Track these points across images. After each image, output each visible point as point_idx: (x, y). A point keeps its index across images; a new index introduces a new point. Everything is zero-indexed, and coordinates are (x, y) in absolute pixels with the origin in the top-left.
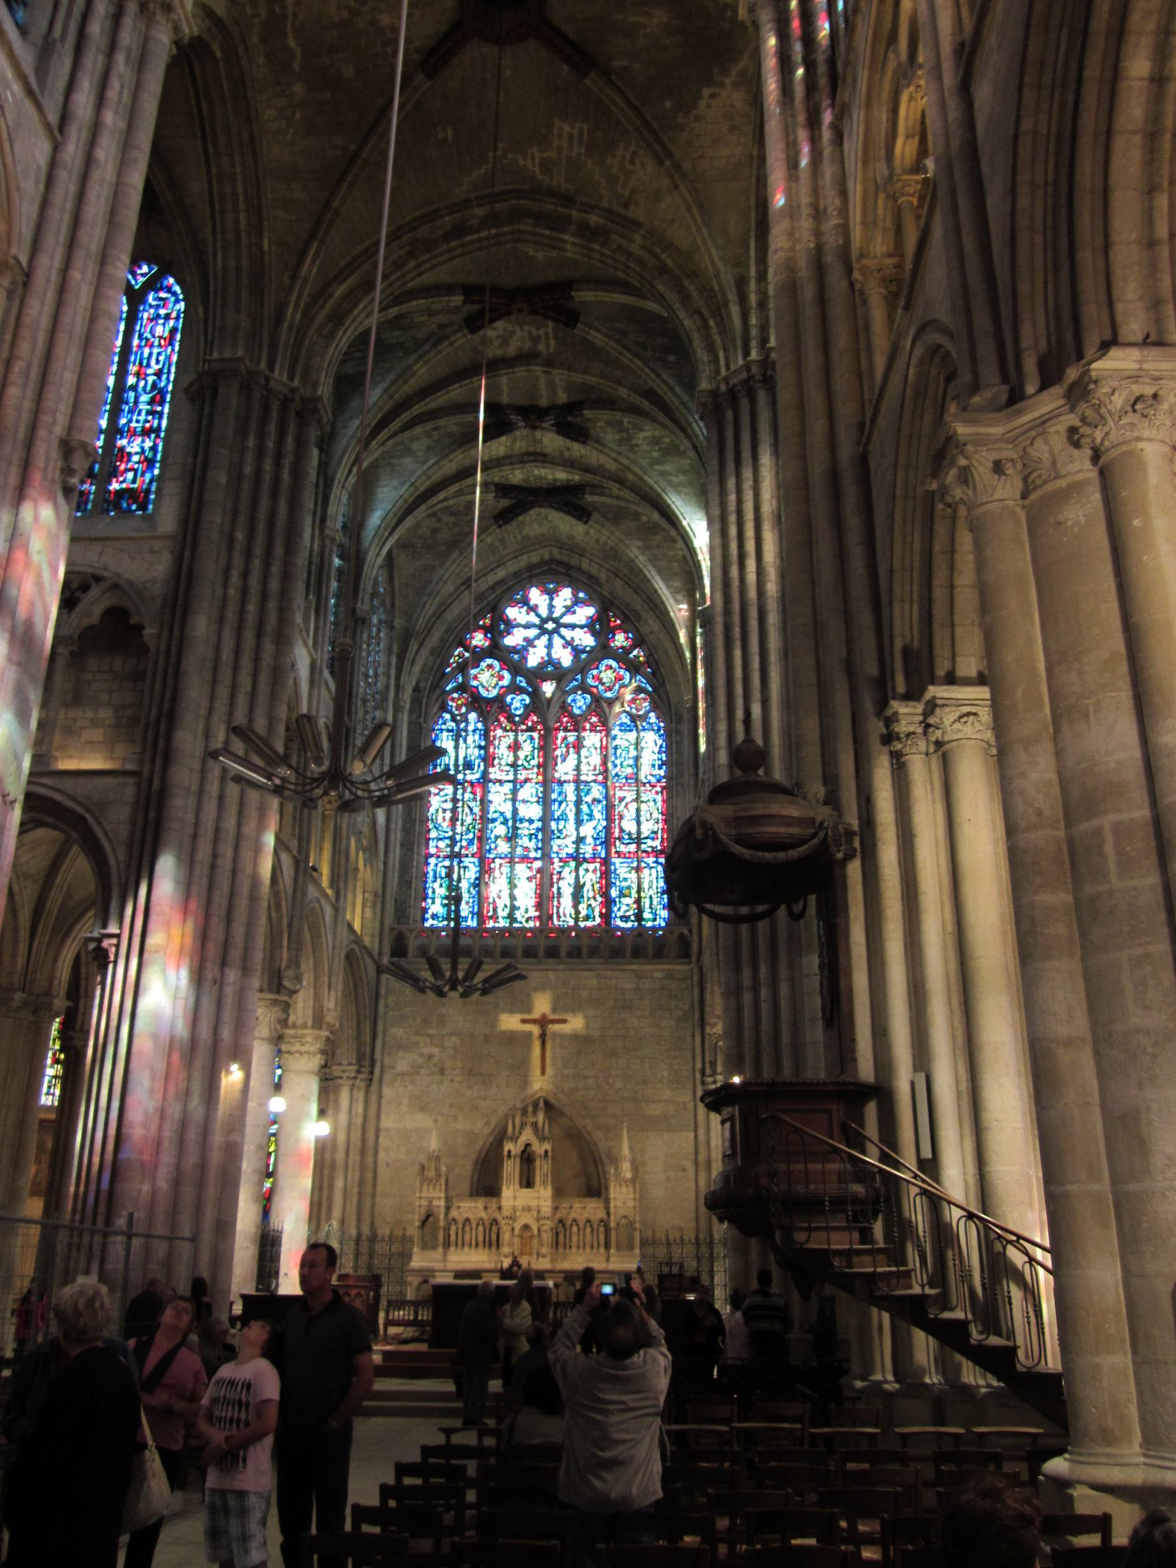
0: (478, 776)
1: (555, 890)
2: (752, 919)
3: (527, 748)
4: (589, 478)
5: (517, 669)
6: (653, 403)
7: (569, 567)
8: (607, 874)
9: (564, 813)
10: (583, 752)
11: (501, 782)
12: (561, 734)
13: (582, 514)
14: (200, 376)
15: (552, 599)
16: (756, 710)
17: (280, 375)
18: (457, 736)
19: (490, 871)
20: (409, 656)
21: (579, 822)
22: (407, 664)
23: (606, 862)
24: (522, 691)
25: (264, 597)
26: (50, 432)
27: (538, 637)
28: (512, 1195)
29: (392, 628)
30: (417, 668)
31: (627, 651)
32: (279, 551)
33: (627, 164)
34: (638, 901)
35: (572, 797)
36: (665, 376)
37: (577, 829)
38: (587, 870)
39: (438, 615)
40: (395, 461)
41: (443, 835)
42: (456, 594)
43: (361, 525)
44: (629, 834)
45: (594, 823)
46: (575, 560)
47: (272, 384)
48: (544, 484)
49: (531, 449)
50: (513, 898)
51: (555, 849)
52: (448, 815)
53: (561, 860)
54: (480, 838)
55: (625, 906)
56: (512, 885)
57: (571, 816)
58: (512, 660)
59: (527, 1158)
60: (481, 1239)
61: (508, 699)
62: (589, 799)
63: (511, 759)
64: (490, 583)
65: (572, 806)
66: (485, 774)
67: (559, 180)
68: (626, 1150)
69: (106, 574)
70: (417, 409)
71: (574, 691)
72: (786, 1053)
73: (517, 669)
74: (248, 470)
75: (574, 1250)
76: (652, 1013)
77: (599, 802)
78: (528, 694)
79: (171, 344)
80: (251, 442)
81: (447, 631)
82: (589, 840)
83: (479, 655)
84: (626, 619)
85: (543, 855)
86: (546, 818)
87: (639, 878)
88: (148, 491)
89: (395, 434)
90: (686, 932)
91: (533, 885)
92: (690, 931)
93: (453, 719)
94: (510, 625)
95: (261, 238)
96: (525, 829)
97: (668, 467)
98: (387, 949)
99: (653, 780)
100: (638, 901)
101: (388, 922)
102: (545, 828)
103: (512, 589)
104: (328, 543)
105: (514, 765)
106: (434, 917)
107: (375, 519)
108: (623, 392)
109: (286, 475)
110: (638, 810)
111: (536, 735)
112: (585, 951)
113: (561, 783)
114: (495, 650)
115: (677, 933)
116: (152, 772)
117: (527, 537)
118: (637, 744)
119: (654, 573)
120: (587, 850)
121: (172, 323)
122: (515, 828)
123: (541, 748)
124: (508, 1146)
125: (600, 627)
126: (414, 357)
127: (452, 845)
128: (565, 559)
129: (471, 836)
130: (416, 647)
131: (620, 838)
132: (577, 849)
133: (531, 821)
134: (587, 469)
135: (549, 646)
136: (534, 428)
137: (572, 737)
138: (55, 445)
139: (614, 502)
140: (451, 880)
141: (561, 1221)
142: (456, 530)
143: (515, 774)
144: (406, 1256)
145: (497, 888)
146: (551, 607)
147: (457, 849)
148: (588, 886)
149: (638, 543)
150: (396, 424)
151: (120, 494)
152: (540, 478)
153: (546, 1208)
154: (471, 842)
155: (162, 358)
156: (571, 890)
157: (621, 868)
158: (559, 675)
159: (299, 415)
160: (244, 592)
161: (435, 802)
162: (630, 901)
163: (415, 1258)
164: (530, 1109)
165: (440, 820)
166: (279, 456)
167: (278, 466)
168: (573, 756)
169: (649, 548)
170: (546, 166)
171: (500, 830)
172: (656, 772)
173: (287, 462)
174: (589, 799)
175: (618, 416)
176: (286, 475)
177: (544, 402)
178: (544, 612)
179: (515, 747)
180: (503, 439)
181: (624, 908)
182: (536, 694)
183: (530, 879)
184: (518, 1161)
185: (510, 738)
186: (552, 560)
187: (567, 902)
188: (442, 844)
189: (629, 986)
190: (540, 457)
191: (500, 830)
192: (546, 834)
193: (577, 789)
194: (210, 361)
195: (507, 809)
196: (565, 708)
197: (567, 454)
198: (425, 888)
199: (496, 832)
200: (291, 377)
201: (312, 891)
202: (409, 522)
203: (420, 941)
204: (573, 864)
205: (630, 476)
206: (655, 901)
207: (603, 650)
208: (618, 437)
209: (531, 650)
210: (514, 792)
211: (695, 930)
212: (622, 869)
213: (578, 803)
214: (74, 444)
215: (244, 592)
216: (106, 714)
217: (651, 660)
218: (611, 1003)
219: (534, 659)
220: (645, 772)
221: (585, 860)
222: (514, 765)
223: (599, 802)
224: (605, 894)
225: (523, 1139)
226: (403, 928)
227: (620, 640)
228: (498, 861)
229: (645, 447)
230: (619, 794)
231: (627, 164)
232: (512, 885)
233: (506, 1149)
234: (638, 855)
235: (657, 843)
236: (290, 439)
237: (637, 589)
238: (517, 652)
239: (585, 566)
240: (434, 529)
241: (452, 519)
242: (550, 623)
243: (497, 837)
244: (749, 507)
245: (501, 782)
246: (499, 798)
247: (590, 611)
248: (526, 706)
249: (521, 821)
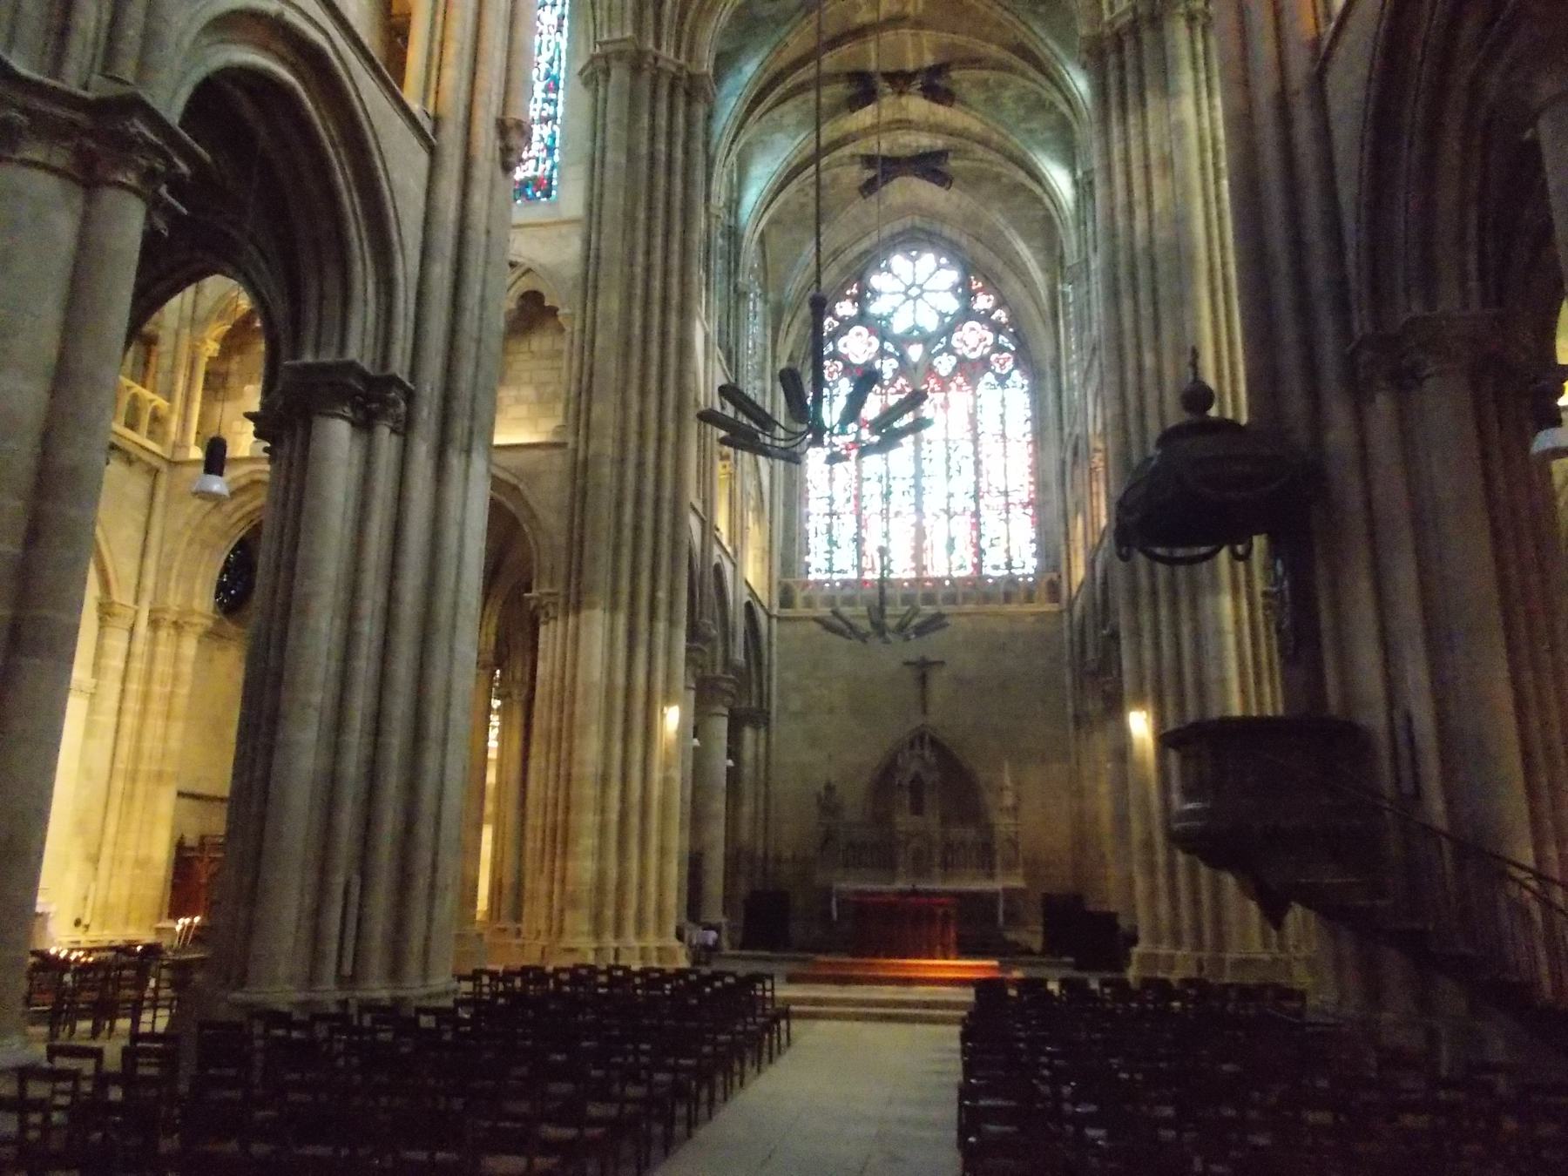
2: (1192, 561)
4: (954, 141)
5: (883, 336)
6: (1023, 58)
7: (930, 234)
13: (942, 179)
14: (593, 59)
16: (1149, 360)
17: (667, 52)
20: (784, 326)
22: (782, 334)
24: (891, 355)
25: (666, 274)
26: (488, 112)
29: (766, 302)
30: (791, 338)
31: (989, 313)
32: (677, 229)
36: (1036, 29)
40: (766, 138)
43: (738, 202)
46: (937, 227)
47: (661, 63)
48: (907, 152)
49: (898, 116)
58: (880, 329)
68: (1007, 781)
69: (519, 260)
70: (790, 83)
71: (939, 353)
72: (1190, 691)
74: (644, 149)
79: (559, 31)
80: (645, 121)
83: (846, 325)
84: (986, 279)
88: (550, 179)
89: (770, 109)
94: (876, 294)
96: (897, 487)
97: (1034, 125)
98: (776, 601)
101: (776, 574)
103: (871, 259)
104: (713, 220)
106: (818, 570)
108: (993, 50)
109: (679, 154)
112: (960, 599)
114: (862, 318)
116: (577, 442)
120: (956, 505)
121: (558, 10)
122: (889, 487)
125: (966, 294)
126: (787, 27)
128: (927, 227)
134: (951, 133)
136: (901, 93)
138: (492, 122)
139: (977, 164)
150: (770, 99)
151: (524, 184)
152: (905, 146)
155: (552, 45)
158: (927, 340)
159: (688, 94)
160: (648, 269)
164: (917, 743)
166: (670, 135)
167: (670, 144)
173: (679, 141)
175: (985, 74)
176: (679, 154)
177: (910, 67)
180: (870, 108)
182: (902, 359)
186: (913, 228)
190: (905, 124)
194: (601, 44)
196: (931, 370)
197: (932, 119)
200: (677, 55)
201: (716, 551)
202: (782, 197)
203: (805, 593)
205: (995, 137)
207: (967, 314)
208: (983, 97)
211: (1064, 577)
212: (992, 525)
214: (509, 123)
215: (648, 269)
216: (528, 392)
217: (1014, 318)
226: (790, 581)
227: (983, 302)
229: (1011, 105)
236: (680, 119)
237: (998, 253)
240: (810, 197)
242: (914, 288)
244: (1135, 153)
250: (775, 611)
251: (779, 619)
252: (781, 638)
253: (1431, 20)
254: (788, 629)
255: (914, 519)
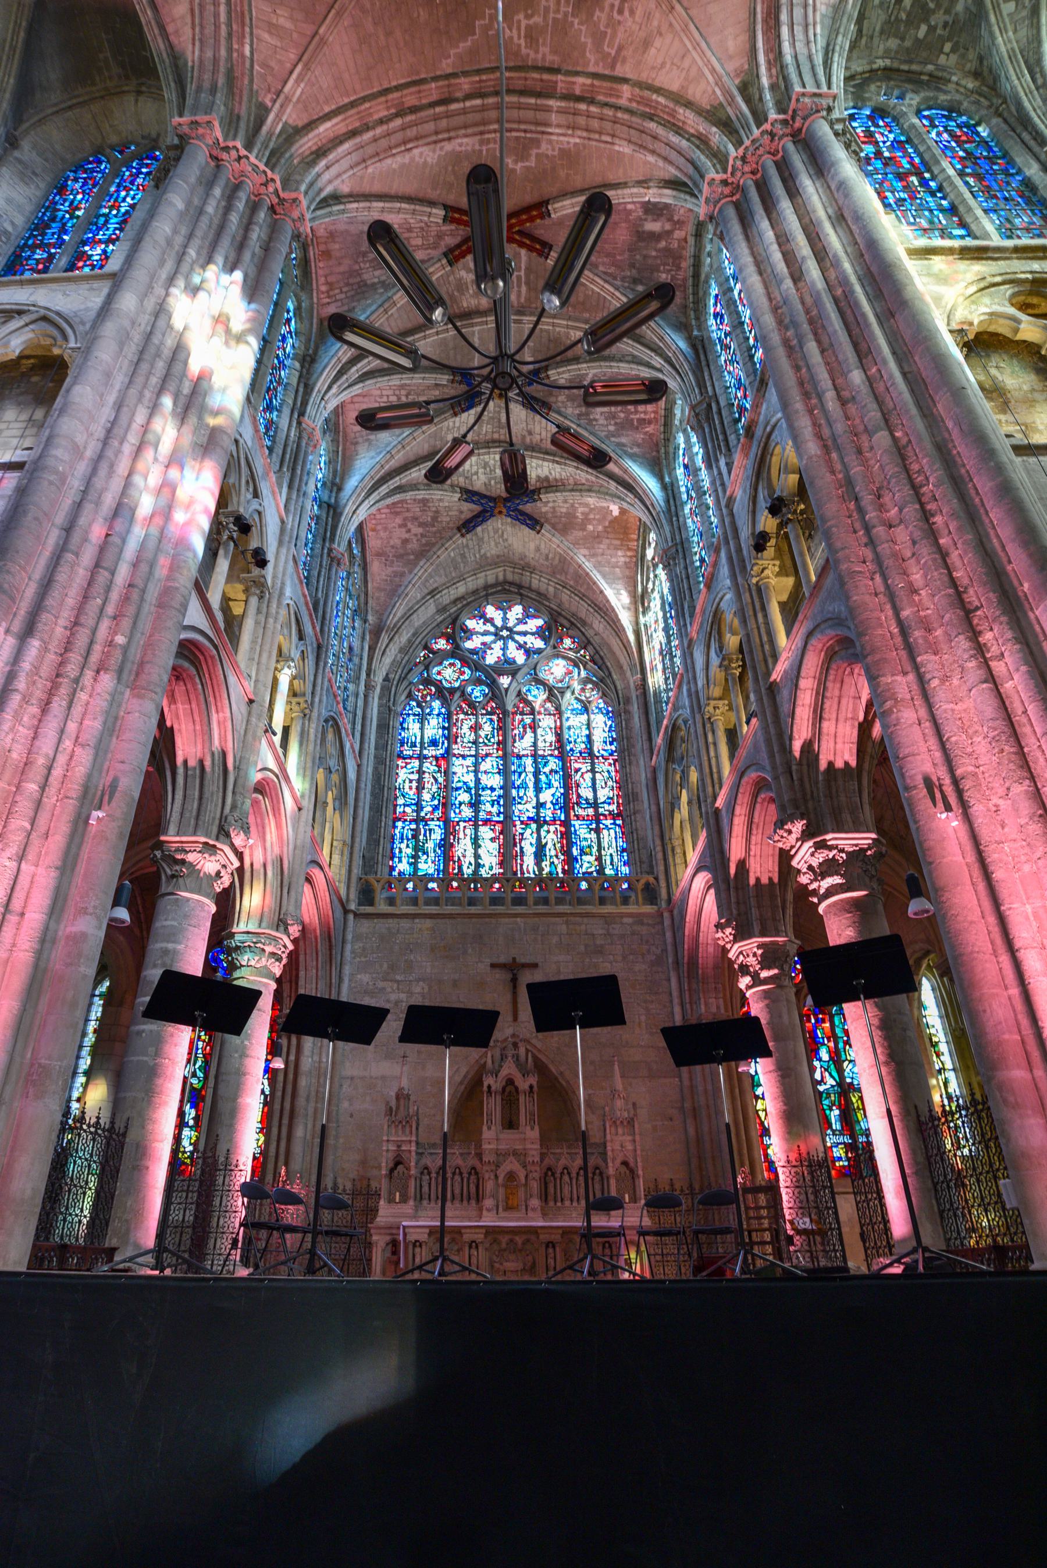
0: (442, 751)
1: (518, 849)
3: (487, 728)
5: (477, 667)
8: (567, 836)
9: (524, 782)
10: (539, 731)
11: (464, 757)
12: (518, 717)
15: (505, 614)
18: (422, 719)
19: (455, 833)
21: (538, 790)
23: (566, 824)
27: (494, 642)
28: (492, 1137)
33: (615, 14)
34: (599, 859)
35: (530, 769)
37: (537, 796)
38: (548, 832)
39: (407, 616)
41: (409, 801)
42: (422, 602)
44: (587, 800)
45: (552, 790)
50: (477, 856)
51: (517, 813)
52: (414, 784)
53: (522, 822)
54: (444, 805)
55: (587, 864)
56: (476, 843)
57: (531, 785)
58: (471, 661)
59: (510, 1093)
60: (457, 1191)
61: (469, 689)
62: (547, 770)
63: (472, 737)
64: (452, 598)
65: (531, 776)
66: (448, 750)
67: (545, 54)
73: (477, 667)
75: (567, 1203)
76: (624, 958)
77: (556, 772)
78: (488, 685)
81: (414, 635)
82: (549, 805)
83: (440, 657)
85: (505, 818)
86: (506, 787)
87: (599, 838)
90: (651, 879)
91: (496, 845)
92: (656, 879)
93: (419, 705)
94: (469, 634)
95: (243, 45)
96: (486, 796)
98: (353, 895)
99: (606, 754)
100: (599, 859)
101: (356, 871)
102: (506, 795)
105: (475, 742)
107: (352, 483)
110: (594, 780)
111: (495, 718)
113: (519, 757)
114: (456, 652)
115: (643, 881)
117: (484, 557)
118: (588, 725)
119: (599, 577)
120: (547, 813)
123: (500, 728)
124: (488, 1081)
127: (418, 812)
128: (517, 578)
129: (436, 802)
130: (386, 641)
131: (578, 804)
132: (538, 813)
133: (492, 789)
135: (504, 649)
137: (528, 720)
140: (417, 841)
141: (549, 1169)
142: (424, 541)
143: (477, 750)
144: (372, 1212)
145: (463, 847)
146: (505, 619)
147: (423, 814)
148: (550, 845)
149: (585, 552)
153: (534, 1150)
154: (436, 808)
156: (534, 849)
157: (582, 831)
161: (403, 774)
162: (592, 859)
163: (381, 1212)
165: (407, 790)
168: (529, 735)
169: (594, 555)
170: (532, 36)
171: (464, 797)
172: (609, 747)
174: (547, 770)
178: (499, 623)
179: (476, 728)
181: (586, 865)
182: (493, 685)
183: (493, 840)
184: (499, 1098)
185: (471, 721)
187: (529, 861)
188: (408, 810)
189: (601, 932)
191: (464, 797)
192: (507, 800)
193: (535, 762)
195: (470, 778)
198: (392, 848)
199: (461, 798)
204: (534, 826)
206: (615, 860)
209: (489, 652)
210: (476, 765)
213: (537, 774)
218: (582, 948)
219: (491, 659)
220: (598, 746)
221: (545, 822)
222: (475, 742)
223: (556, 772)
224: (567, 851)
225: (504, 1072)
228: (462, 824)
229: (602, 421)
230: (577, 766)
231: (615, 14)
232: (476, 843)
233: (486, 1084)
234: (597, 818)
235: (613, 807)
238: (477, 653)
239: (535, 584)
241: (420, 530)
243: (460, 804)
245: (464, 757)
246: (462, 771)
247: (540, 622)
248: (485, 695)
249: (483, 789)
250: (353, 906)
251: (356, 915)
252: (357, 938)
253: (900, 452)
254: (365, 926)
255: (480, 851)
